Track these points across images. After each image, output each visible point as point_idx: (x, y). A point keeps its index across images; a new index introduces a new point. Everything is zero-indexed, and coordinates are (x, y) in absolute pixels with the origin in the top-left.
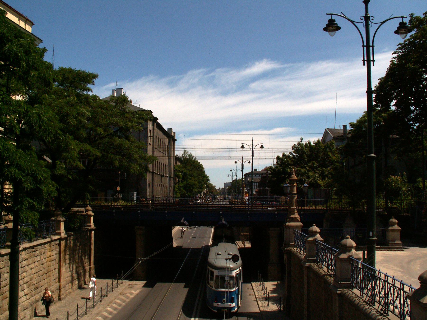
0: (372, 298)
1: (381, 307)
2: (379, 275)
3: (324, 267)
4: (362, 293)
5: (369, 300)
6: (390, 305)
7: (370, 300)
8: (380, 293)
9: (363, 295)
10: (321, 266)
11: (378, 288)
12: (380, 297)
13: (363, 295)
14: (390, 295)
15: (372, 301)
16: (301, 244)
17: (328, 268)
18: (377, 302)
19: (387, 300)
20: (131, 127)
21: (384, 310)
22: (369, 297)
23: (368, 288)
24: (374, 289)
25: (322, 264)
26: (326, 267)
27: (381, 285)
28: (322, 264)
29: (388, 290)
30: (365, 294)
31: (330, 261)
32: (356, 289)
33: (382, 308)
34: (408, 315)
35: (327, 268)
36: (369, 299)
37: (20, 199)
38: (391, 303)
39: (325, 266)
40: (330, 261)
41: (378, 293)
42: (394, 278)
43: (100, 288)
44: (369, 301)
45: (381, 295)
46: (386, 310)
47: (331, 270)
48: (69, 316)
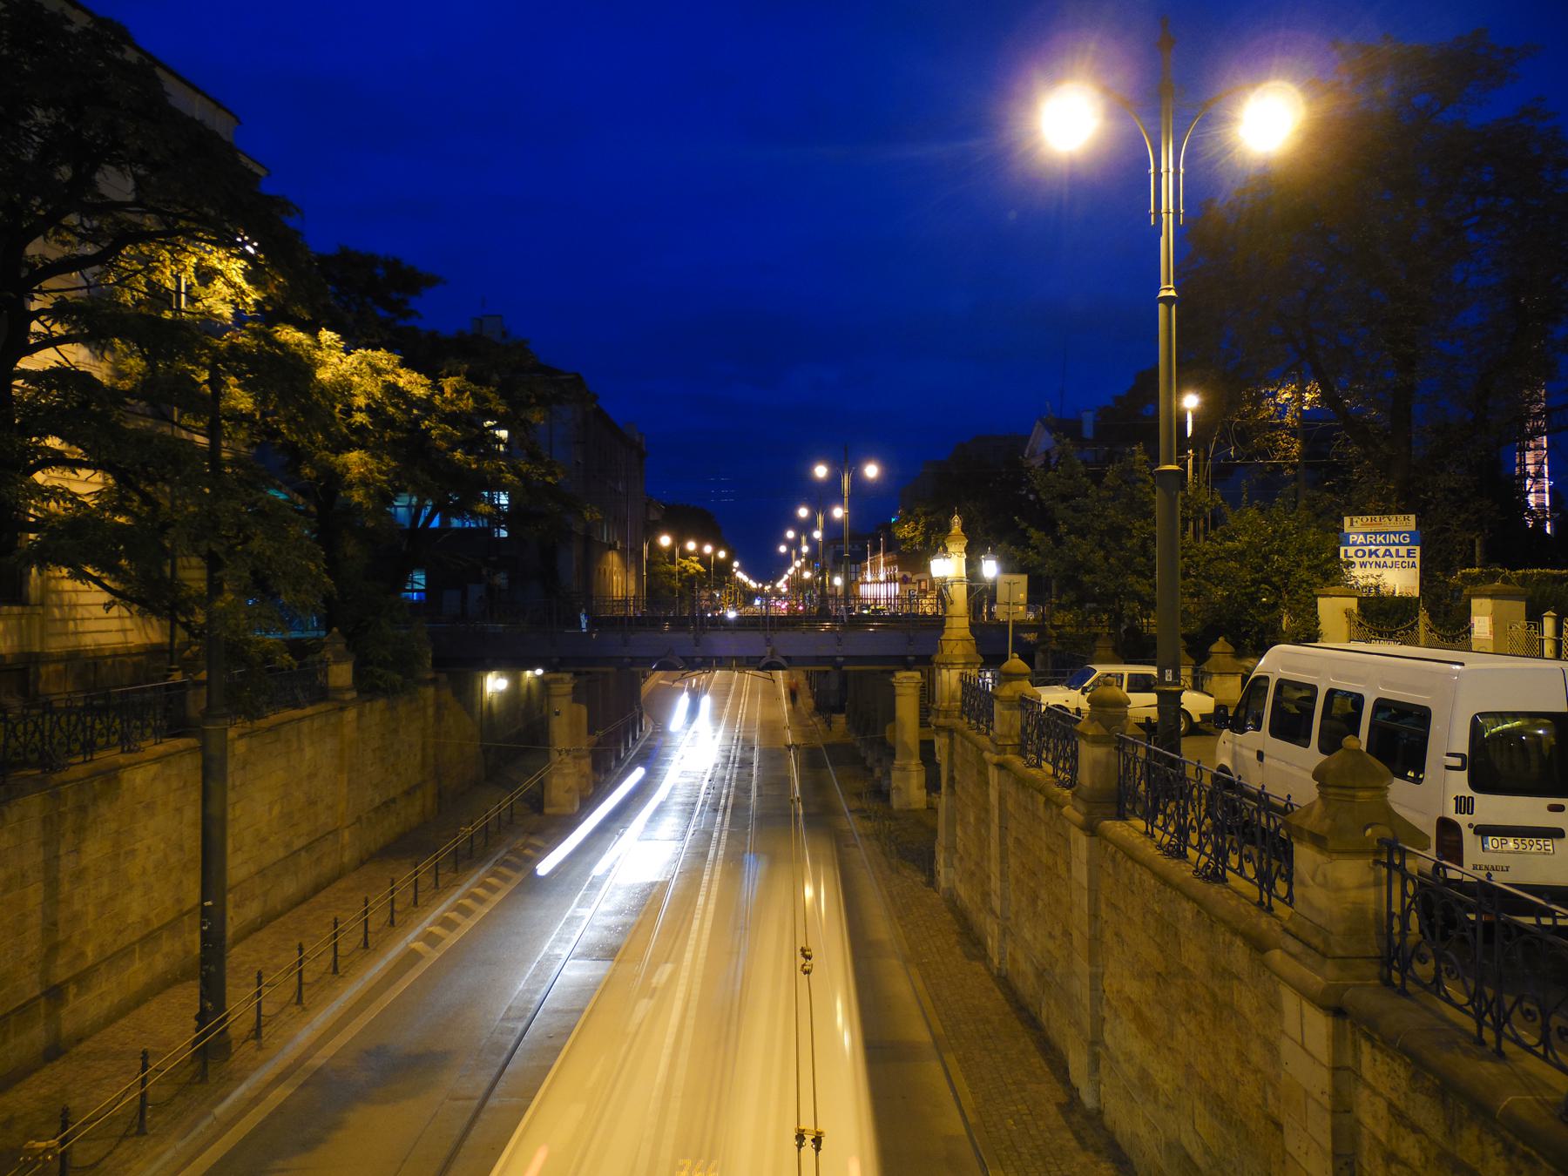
0: (1178, 839)
1: (1204, 859)
2: (1199, 775)
3: (1044, 763)
4: (1265, 894)
5: (1172, 843)
6: (1231, 854)
7: (1173, 843)
8: (1200, 824)
9: (1270, 900)
10: (1035, 761)
11: (1197, 809)
12: (1201, 834)
13: (1270, 900)
14: (1190, 809)
15: (1179, 846)
16: (981, 707)
17: (1055, 766)
18: (1194, 848)
19: (1182, 820)
20: (455, 395)
21: (1212, 866)
22: (1172, 836)
23: (1168, 811)
24: (1186, 812)
25: (1039, 756)
26: (1050, 763)
27: (1138, 771)
28: (1039, 756)
29: (1408, 900)
30: (1160, 828)
31: (1060, 748)
32: (1484, 1037)
33: (1209, 861)
34: (1282, 876)
35: (1053, 766)
36: (1171, 840)
37: (512, 663)
38: (1194, 828)
39: (1046, 760)
40: (1060, 748)
41: (1194, 823)
42: (1291, 801)
43: (256, 974)
44: (1171, 845)
45: (1204, 828)
46: (1220, 866)
47: (1064, 770)
48: (395, 914)
